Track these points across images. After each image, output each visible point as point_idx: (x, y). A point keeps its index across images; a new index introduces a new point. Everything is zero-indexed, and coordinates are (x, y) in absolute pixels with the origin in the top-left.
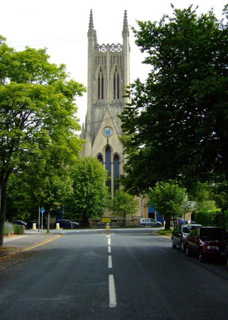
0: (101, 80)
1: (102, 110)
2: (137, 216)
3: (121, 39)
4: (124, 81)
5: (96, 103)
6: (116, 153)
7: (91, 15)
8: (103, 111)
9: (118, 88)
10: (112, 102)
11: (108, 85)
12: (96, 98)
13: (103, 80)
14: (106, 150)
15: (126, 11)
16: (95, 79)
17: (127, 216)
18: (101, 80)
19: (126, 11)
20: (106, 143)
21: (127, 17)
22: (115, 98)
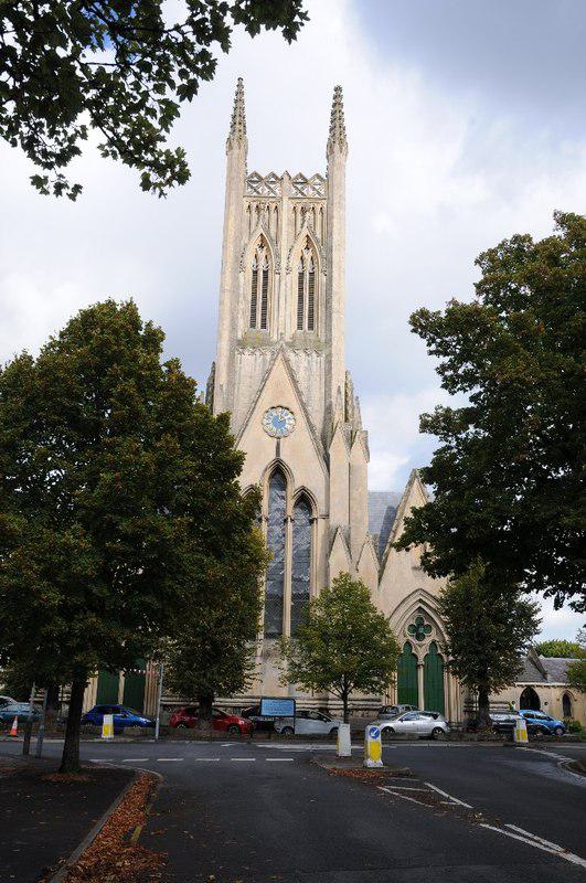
0: (307, 276)
1: (260, 360)
2: (430, 718)
3: (325, 163)
4: (330, 280)
5: (244, 338)
6: (303, 488)
7: (240, 93)
8: (264, 360)
9: (311, 299)
10: (293, 337)
11: (283, 287)
12: (243, 323)
13: (265, 273)
14: (272, 476)
15: (338, 89)
16: (242, 268)
17: (350, 696)
18: (307, 276)
19: (338, 89)
20: (273, 456)
21: (242, 93)
22: (300, 326)
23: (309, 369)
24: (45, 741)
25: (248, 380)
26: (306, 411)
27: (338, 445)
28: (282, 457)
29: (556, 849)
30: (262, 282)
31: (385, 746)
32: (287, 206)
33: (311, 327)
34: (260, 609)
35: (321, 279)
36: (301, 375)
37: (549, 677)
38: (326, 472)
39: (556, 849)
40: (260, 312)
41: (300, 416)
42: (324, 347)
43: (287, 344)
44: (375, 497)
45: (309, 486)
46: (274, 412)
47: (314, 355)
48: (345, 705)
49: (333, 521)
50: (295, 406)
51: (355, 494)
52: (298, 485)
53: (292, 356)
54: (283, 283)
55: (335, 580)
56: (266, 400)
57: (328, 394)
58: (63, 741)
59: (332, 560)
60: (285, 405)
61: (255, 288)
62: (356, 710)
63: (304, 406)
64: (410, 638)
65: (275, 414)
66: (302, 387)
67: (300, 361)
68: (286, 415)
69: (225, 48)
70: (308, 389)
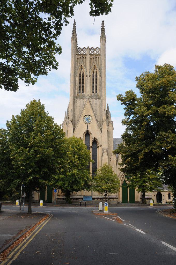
1: (82, 102)
6: (95, 138)
10: (91, 95)
14: (86, 136)
15: (103, 22)
19: (103, 22)
20: (86, 129)
23: (96, 104)
24: (24, 207)
25: (79, 108)
26: (95, 116)
27: (105, 124)
28: (89, 129)
29: (46, 191)
30: (82, 78)
31: (110, 208)
32: (88, 57)
33: (96, 92)
34: (30, 180)
35: (99, 77)
36: (94, 106)
37: (165, 189)
38: (101, 132)
39: (46, 191)
40: (81, 88)
41: (94, 117)
42: (99, 97)
43: (89, 97)
44: (115, 140)
45: (97, 138)
46: (86, 117)
47: (98, 100)
48: (106, 197)
49: (103, 147)
50: (92, 115)
51: (110, 139)
52: (93, 137)
53: (91, 100)
54: (88, 79)
55: (103, 164)
56: (84, 113)
57: (101, 111)
58: (28, 207)
59: (103, 158)
60: (89, 115)
61: (80, 79)
62: (111, 199)
63: (95, 115)
64: (125, 179)
65: (86, 117)
66: (94, 109)
67: (94, 102)
68: (90, 117)
69: (66, 25)
70: (96, 109)
